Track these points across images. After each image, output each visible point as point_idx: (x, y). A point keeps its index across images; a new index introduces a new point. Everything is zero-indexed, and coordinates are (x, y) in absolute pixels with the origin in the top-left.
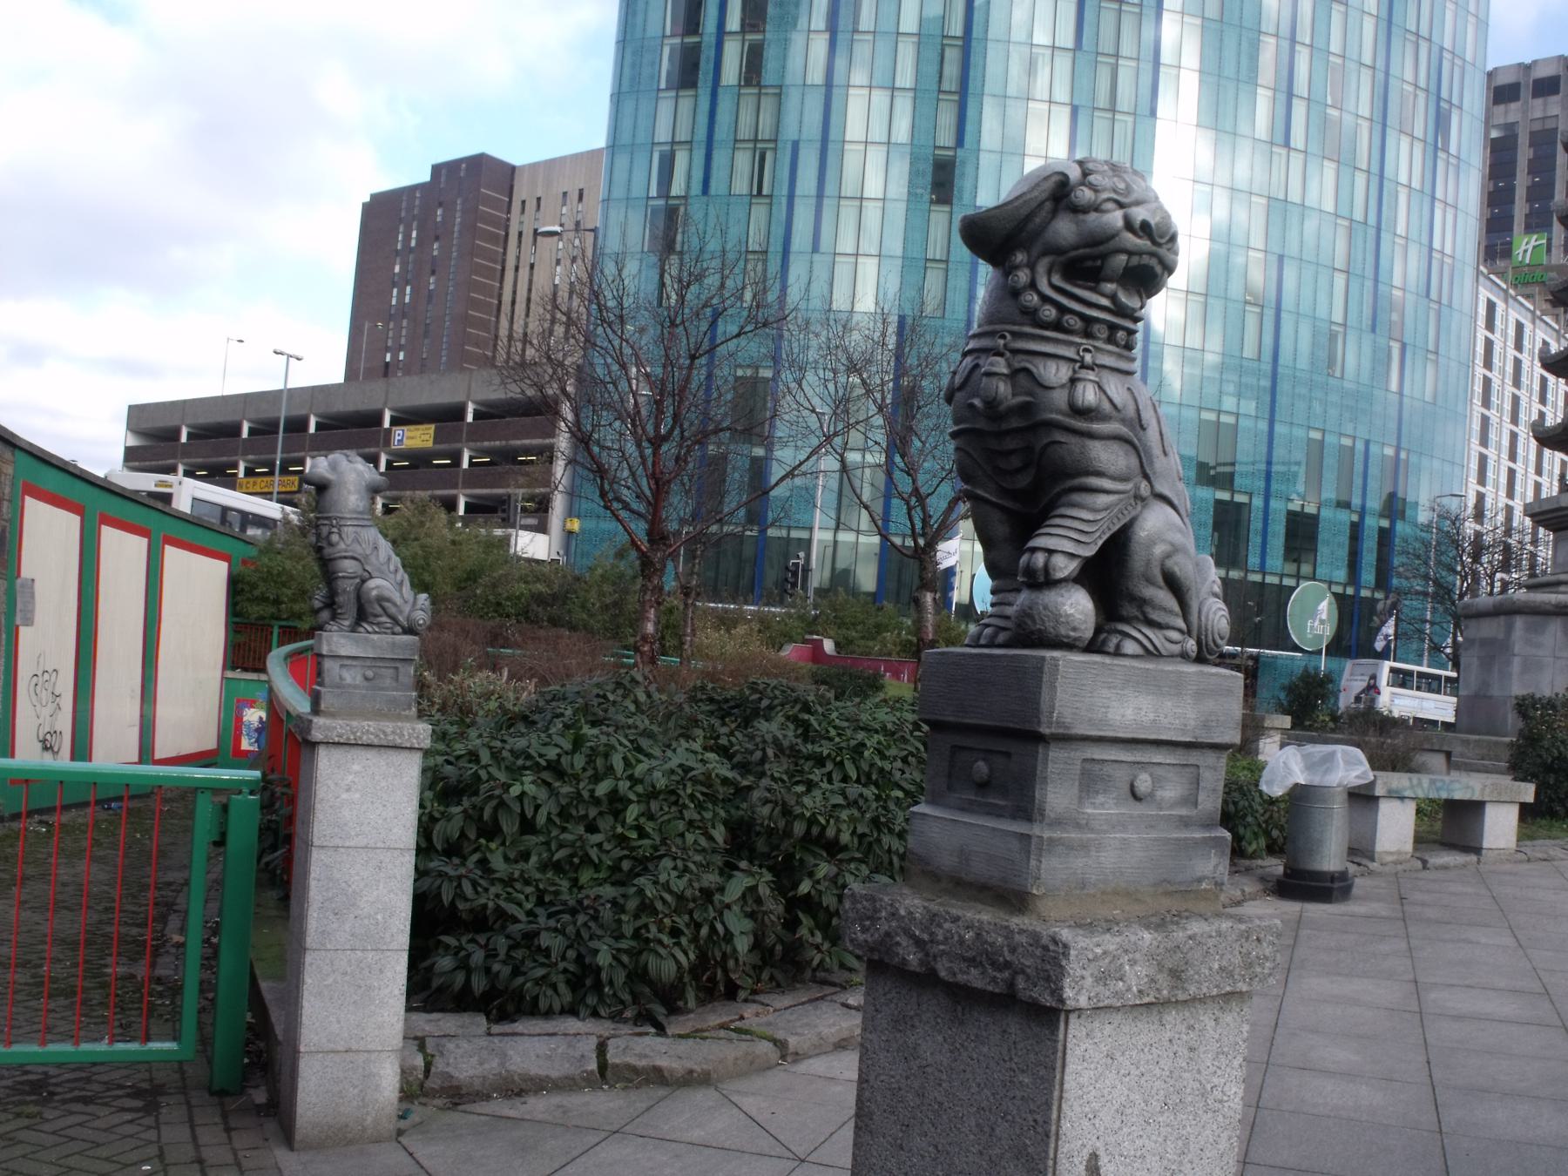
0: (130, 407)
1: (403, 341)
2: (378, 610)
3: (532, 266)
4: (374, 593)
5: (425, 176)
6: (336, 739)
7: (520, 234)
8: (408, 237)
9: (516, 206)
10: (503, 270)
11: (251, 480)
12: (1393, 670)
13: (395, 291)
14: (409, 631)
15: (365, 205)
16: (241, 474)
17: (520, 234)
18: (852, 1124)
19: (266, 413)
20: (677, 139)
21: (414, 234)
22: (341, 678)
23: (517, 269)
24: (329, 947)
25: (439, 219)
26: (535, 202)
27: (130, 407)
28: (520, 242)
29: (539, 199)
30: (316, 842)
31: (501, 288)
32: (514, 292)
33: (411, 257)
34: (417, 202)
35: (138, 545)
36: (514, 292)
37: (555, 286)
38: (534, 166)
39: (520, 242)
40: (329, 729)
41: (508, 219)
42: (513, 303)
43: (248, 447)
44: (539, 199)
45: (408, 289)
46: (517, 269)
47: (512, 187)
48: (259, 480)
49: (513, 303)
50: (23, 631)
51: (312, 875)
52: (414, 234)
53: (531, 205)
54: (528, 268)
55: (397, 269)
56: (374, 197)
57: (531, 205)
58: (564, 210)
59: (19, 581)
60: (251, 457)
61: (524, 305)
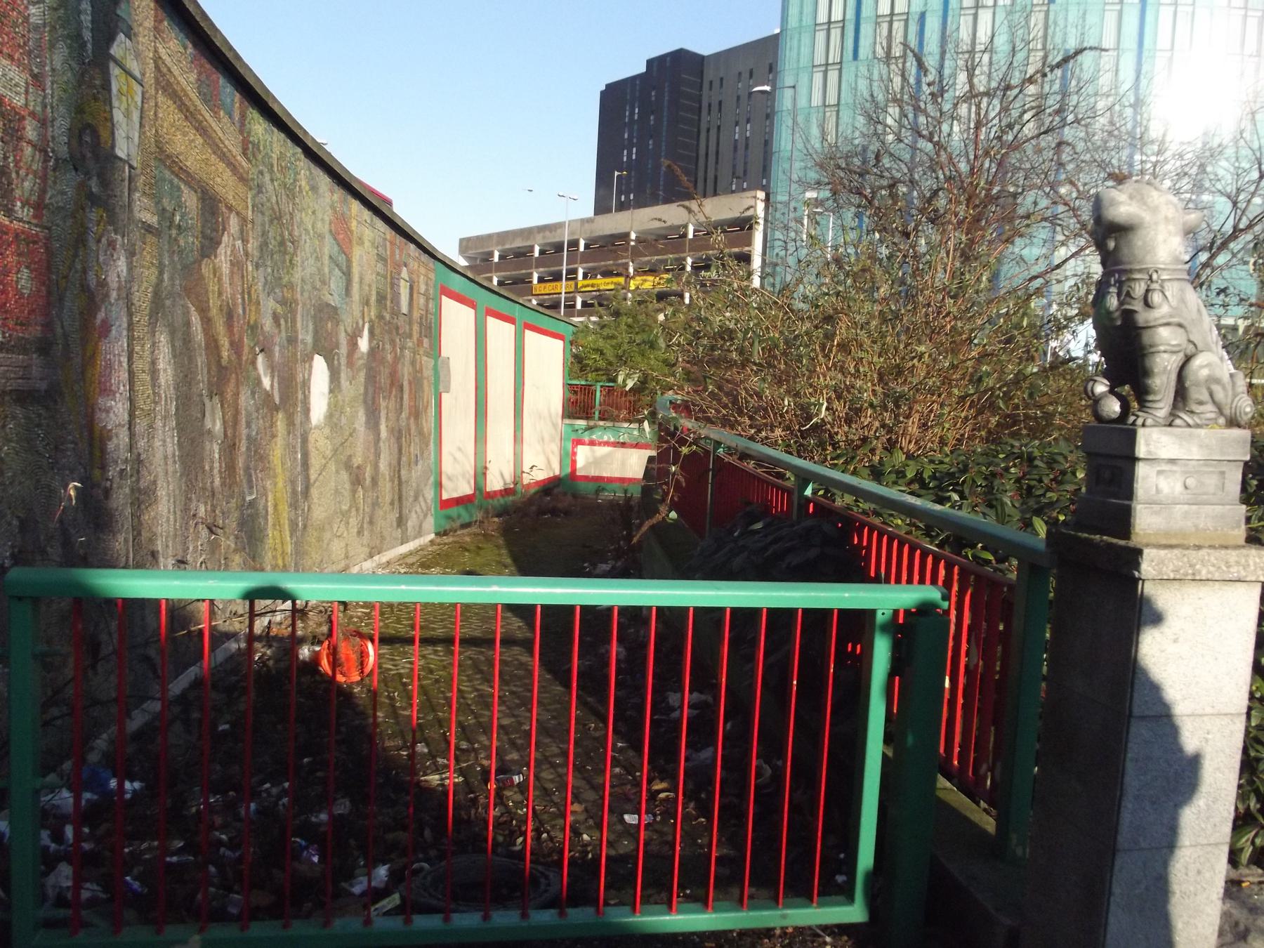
0: (461, 241)
1: (632, 186)
2: (1205, 396)
3: (719, 127)
4: (1204, 373)
5: (642, 69)
6: (1172, 576)
7: (710, 105)
8: (632, 113)
9: (706, 86)
10: (699, 132)
11: (543, 285)
12: (602, 387)
13: (625, 152)
14: (1233, 423)
15: (602, 93)
16: (535, 280)
17: (710, 105)
18: (312, 481)
19: (553, 238)
20: (833, 20)
21: (637, 111)
22: (1158, 491)
23: (708, 130)
24: (1143, 845)
25: (653, 99)
26: (719, 82)
27: (461, 241)
28: (710, 110)
29: (722, 79)
30: (1136, 711)
31: (698, 145)
32: (707, 147)
33: (636, 127)
34: (638, 88)
35: (509, 328)
36: (707, 147)
37: (747, 138)
38: (718, 55)
39: (710, 110)
40: (1162, 562)
41: (701, 95)
42: (707, 154)
43: (540, 263)
44: (722, 79)
45: (634, 150)
46: (708, 130)
47: (702, 72)
48: (548, 284)
49: (707, 154)
50: (444, 396)
51: (1129, 755)
52: (637, 111)
53: (716, 84)
54: (715, 130)
55: (626, 136)
56: (608, 86)
57: (716, 84)
58: (740, 85)
59: (440, 360)
60: (541, 269)
61: (714, 157)
